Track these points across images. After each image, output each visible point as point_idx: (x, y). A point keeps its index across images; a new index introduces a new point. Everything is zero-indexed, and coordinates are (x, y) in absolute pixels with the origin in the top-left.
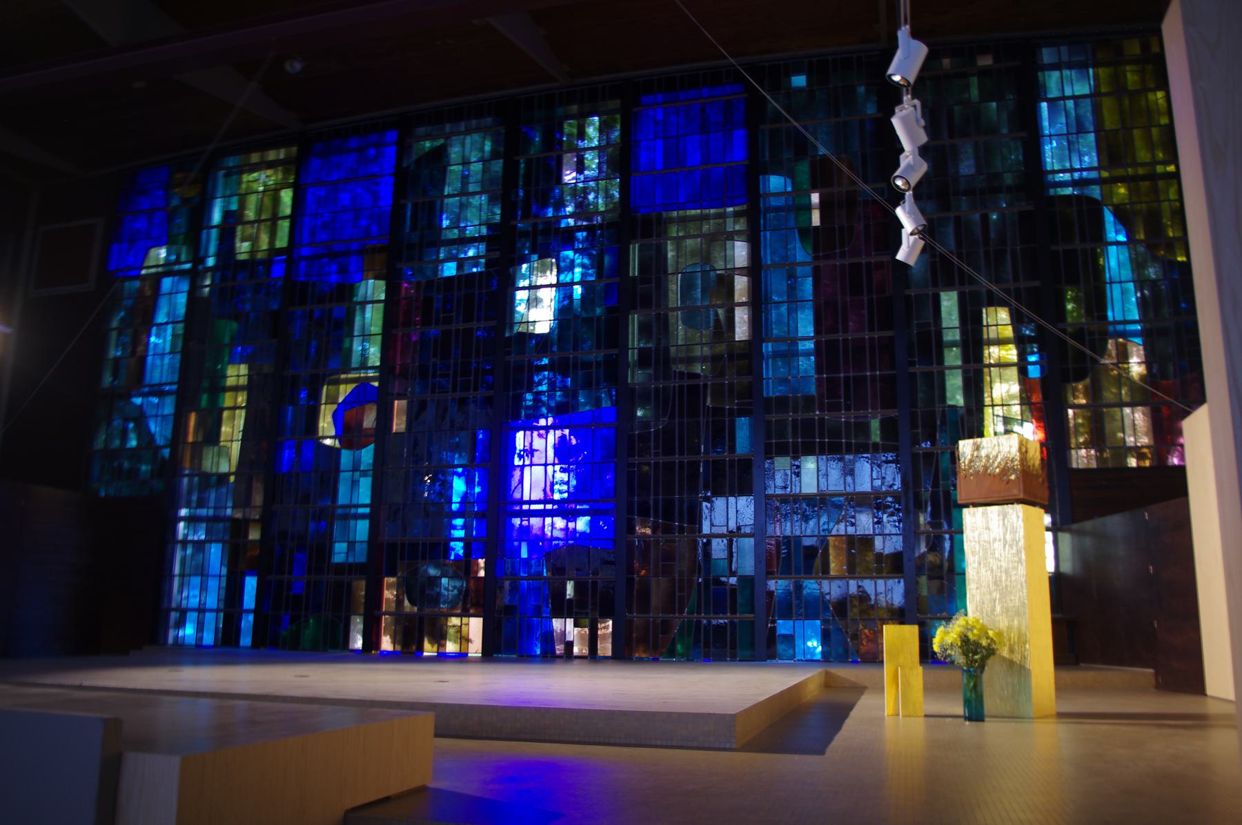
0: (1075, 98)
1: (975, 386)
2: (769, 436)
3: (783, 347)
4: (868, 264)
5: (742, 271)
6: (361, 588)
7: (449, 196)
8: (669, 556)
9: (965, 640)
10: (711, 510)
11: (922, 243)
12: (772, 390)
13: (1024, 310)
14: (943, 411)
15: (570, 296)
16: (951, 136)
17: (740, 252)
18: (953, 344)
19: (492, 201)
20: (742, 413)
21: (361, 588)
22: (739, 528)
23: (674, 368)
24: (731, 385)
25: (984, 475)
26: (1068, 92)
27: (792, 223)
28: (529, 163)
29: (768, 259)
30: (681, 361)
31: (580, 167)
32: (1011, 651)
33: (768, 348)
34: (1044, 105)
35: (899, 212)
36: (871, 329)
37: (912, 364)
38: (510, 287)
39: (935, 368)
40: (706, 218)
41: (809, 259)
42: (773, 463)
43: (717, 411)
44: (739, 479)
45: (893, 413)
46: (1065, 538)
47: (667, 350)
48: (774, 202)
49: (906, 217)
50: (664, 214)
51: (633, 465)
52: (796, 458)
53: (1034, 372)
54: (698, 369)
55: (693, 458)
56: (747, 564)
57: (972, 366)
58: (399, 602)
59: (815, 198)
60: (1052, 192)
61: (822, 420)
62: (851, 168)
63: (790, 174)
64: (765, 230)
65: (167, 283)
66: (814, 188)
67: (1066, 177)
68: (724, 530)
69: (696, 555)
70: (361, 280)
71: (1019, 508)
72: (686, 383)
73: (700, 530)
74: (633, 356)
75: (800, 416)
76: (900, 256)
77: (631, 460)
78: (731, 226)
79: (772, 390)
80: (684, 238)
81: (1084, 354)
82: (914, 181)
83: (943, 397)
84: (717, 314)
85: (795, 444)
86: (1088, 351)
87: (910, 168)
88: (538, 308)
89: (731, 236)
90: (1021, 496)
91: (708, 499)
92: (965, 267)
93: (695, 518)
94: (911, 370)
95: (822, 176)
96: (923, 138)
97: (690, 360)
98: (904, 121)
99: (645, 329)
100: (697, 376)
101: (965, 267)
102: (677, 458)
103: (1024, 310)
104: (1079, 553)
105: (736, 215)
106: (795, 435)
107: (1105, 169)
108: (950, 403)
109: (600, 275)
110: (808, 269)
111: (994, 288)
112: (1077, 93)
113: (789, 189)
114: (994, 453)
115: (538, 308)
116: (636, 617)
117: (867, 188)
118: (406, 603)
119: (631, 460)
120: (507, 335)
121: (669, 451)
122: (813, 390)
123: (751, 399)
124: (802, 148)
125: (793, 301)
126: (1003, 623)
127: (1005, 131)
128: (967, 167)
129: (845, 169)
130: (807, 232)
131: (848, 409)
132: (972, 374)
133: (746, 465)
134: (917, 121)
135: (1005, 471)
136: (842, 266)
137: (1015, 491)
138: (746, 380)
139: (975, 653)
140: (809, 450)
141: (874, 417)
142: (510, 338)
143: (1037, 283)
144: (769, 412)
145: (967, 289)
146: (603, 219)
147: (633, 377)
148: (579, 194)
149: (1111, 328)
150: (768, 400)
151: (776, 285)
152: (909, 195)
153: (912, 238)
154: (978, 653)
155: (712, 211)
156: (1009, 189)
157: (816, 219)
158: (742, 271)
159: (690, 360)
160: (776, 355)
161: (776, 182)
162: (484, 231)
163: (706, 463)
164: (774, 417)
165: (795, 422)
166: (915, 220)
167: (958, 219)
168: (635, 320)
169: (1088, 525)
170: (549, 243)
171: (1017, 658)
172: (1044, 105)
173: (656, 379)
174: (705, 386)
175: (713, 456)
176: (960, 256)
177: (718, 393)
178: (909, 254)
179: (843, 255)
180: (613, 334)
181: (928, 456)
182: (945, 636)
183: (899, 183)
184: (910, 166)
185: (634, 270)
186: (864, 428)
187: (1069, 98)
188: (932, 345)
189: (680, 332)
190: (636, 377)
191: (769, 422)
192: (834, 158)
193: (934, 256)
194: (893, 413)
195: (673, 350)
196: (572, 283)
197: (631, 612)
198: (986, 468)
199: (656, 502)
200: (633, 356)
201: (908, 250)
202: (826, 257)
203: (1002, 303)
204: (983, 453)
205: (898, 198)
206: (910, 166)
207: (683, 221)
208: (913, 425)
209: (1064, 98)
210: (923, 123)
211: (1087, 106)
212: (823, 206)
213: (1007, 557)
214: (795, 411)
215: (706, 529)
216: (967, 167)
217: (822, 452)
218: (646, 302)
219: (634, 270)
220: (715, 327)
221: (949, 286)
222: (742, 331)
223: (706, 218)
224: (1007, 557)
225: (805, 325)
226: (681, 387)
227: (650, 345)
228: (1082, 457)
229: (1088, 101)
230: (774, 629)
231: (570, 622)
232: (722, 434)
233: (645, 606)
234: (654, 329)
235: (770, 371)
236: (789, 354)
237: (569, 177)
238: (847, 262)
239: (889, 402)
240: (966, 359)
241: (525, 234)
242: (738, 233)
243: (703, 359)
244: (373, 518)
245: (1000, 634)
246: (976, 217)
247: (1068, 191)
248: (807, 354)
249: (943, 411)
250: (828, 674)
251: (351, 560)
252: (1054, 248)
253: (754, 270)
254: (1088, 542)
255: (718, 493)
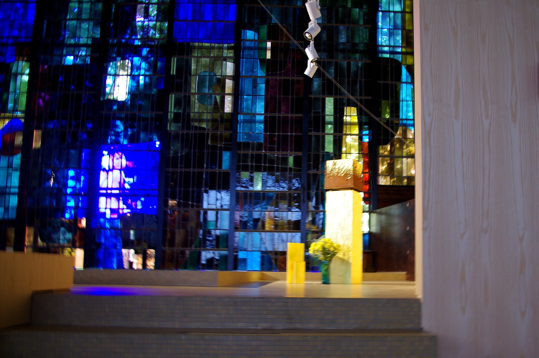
0: (395, 12)
1: (338, 143)
2: (239, 162)
3: (248, 117)
4: (293, 80)
5: (230, 77)
6: (12, 234)
7: (69, 20)
8: (185, 219)
9: (324, 248)
10: (208, 197)
11: (317, 67)
12: (241, 138)
13: (363, 108)
14: (323, 155)
15: (138, 82)
16: (337, 22)
17: (229, 68)
18: (330, 123)
19: (95, 25)
20: (226, 149)
21: (12, 234)
22: (222, 206)
23: (192, 124)
24: (221, 134)
25: (337, 177)
26: (391, 9)
27: (256, 56)
28: (117, 7)
29: (243, 73)
30: (196, 121)
31: (147, 15)
32: (344, 255)
33: (241, 117)
34: (380, 14)
35: (308, 51)
36: (292, 113)
37: (311, 131)
38: (104, 74)
39: (320, 134)
40: (213, 48)
41: (264, 75)
42: (240, 175)
43: (214, 148)
44: (222, 182)
45: (300, 154)
46: (374, 216)
47: (189, 114)
48: (248, 44)
49: (310, 53)
50: (191, 44)
51: (169, 172)
52: (252, 173)
53: (366, 140)
54: (204, 125)
55: (200, 170)
56: (225, 224)
57: (338, 134)
58: (35, 241)
59: (269, 44)
60: (380, 55)
61: (265, 155)
62: (288, 31)
63: (257, 31)
64: (243, 58)
65: (62, 229)
66: (269, 39)
67: (386, 49)
68: (214, 207)
69: (199, 218)
70: (14, 62)
71: (351, 192)
72: (198, 132)
73: (202, 206)
74: (171, 116)
75: (255, 152)
76: (306, 73)
77: (167, 169)
78: (226, 53)
79: (241, 138)
80: (201, 57)
81: (388, 130)
82: (314, 36)
83: (324, 148)
84: (216, 98)
85: (252, 166)
86: (390, 129)
87: (312, 29)
88: (119, 87)
89: (225, 59)
90: (352, 186)
91: (207, 192)
92: (338, 85)
93: (200, 200)
94: (310, 134)
95: (273, 34)
96: (319, 15)
97: (201, 121)
98: (311, 5)
99: (178, 103)
100: (204, 129)
101: (338, 85)
102: (192, 170)
103: (363, 108)
104: (379, 222)
105: (229, 48)
106: (252, 162)
107: (404, 47)
108: (326, 150)
109: (155, 72)
110: (264, 80)
111: (352, 98)
112: (395, 10)
113: (256, 39)
114: (342, 167)
115: (119, 87)
116: (167, 249)
117: (296, 42)
118: (39, 240)
119: (167, 169)
120: (102, 99)
121: (188, 166)
122: (262, 141)
123: (232, 144)
124: (264, 18)
125: (255, 95)
126: (341, 243)
127: (361, 23)
128: (343, 39)
129: (284, 30)
130: (263, 61)
131: (278, 150)
132: (337, 138)
133: (226, 175)
134: (317, 6)
135: (346, 175)
136: (280, 80)
137: (350, 184)
138: (227, 133)
139: (328, 254)
140: (258, 169)
141: (291, 155)
142: (103, 101)
143: (370, 98)
144: (240, 149)
145: (338, 97)
146: (158, 43)
147: (170, 127)
148: (145, 29)
149: (401, 122)
150: (240, 143)
151: (247, 85)
152: (312, 43)
153: (312, 64)
154: (329, 254)
155: (216, 45)
156: (361, 52)
157: (269, 56)
158: (230, 77)
159: (201, 121)
160: (245, 121)
161: (250, 34)
162: (90, 42)
163: (207, 173)
164: (242, 152)
165: (252, 155)
166: (314, 55)
167: (336, 63)
168: (172, 98)
169: (384, 209)
170: (128, 51)
171: (346, 258)
172: (380, 14)
173: (183, 129)
174: (208, 134)
175: (209, 170)
176: (336, 80)
177: (214, 138)
178: (310, 72)
179: (281, 75)
180: (161, 103)
181: (315, 175)
182: (316, 247)
183: (307, 35)
184: (313, 29)
185: (173, 71)
186: (285, 160)
187: (392, 12)
188: (320, 123)
189: (196, 107)
190: (172, 127)
191: (239, 154)
192: (280, 25)
193: (323, 80)
194: (300, 154)
195: (192, 114)
196: (139, 75)
197: (164, 246)
198: (338, 173)
199: (180, 191)
200: (171, 116)
201: (310, 70)
202: (272, 75)
203: (354, 105)
204: (337, 167)
205: (307, 43)
206: (313, 29)
207: (201, 48)
208: (309, 160)
209: (389, 11)
210: (319, 8)
211: (399, 15)
212: (273, 49)
213: (346, 219)
214: (253, 150)
215: (205, 206)
216: (343, 39)
217: (265, 171)
218: (179, 89)
219: (173, 71)
220: (214, 105)
221: (330, 95)
222: (228, 108)
223: (213, 48)
224: (346, 219)
225: (260, 107)
226: (195, 134)
227: (180, 111)
228: (383, 181)
229: (400, 14)
230: (237, 256)
231: (132, 251)
232: (216, 160)
233: (172, 243)
234: (183, 104)
235: (241, 129)
236: (252, 121)
237: (139, 19)
238: (283, 78)
239: (298, 148)
240: (335, 131)
241: (113, 46)
242: (230, 57)
243: (208, 121)
244: (21, 195)
245: (339, 246)
246: (345, 64)
247: (387, 56)
248: (260, 122)
249: (323, 155)
250: (263, 275)
251: (6, 217)
252: (379, 82)
253: (236, 78)
254: (383, 217)
255: (213, 188)
